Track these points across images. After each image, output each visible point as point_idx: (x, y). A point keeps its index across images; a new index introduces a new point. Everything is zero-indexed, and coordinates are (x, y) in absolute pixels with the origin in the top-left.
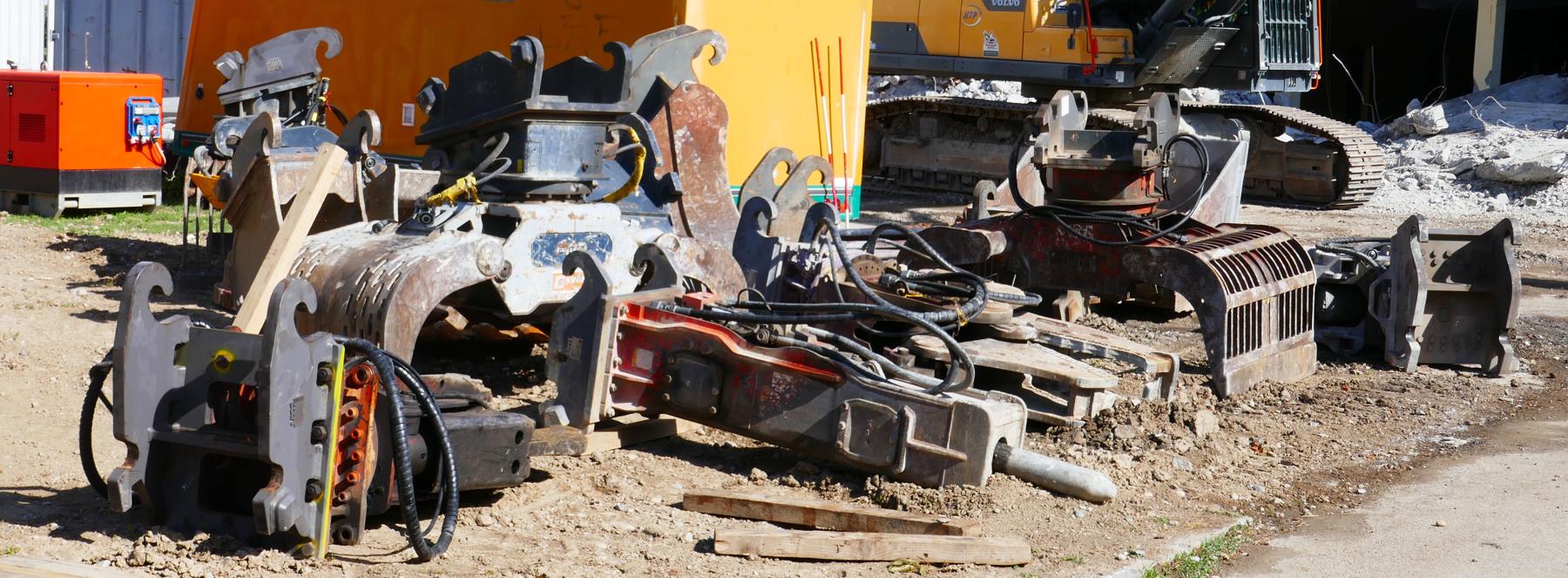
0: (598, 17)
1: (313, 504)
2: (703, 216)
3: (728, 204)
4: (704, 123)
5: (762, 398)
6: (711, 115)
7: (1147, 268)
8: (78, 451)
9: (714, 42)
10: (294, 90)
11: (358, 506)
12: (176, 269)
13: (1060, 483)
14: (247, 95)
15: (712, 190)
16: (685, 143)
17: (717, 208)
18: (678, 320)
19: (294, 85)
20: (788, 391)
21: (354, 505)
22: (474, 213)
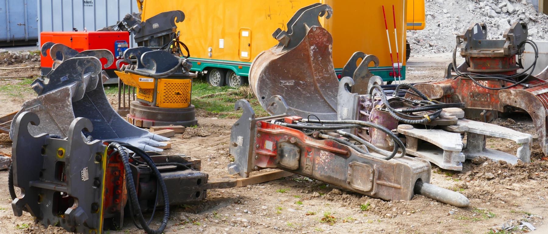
0: (291, 2)
1: (185, 206)
2: (324, 81)
3: (334, 76)
4: (322, 43)
5: (317, 162)
6: (325, 39)
7: (509, 99)
8: (9, 193)
9: (327, 9)
10: (164, 36)
11: (119, 214)
12: (471, 48)
13: (442, 199)
14: (146, 39)
15: (327, 71)
16: (314, 52)
17: (329, 78)
18: (282, 128)
19: (164, 34)
20: (327, 158)
21: (118, 213)
22: (490, 36)
